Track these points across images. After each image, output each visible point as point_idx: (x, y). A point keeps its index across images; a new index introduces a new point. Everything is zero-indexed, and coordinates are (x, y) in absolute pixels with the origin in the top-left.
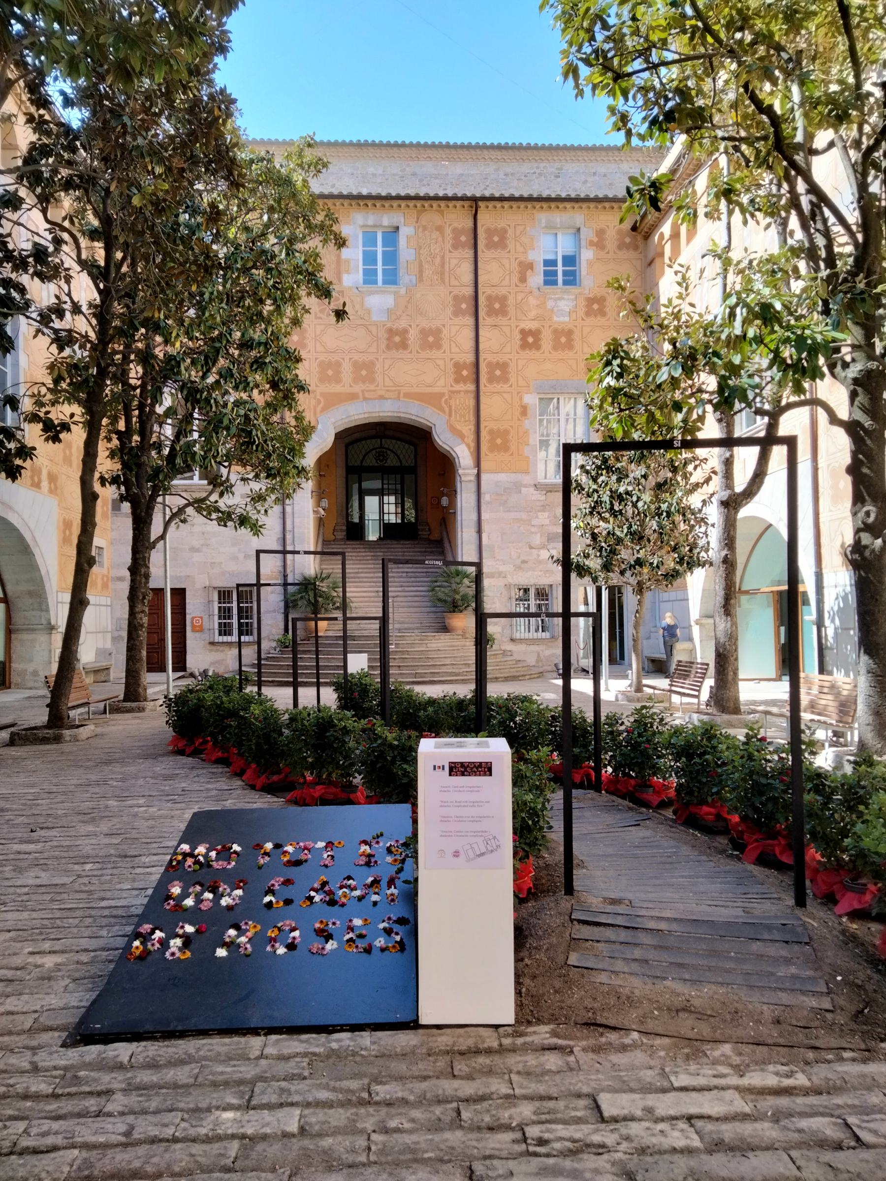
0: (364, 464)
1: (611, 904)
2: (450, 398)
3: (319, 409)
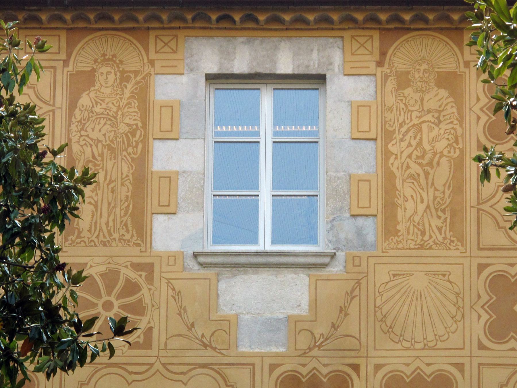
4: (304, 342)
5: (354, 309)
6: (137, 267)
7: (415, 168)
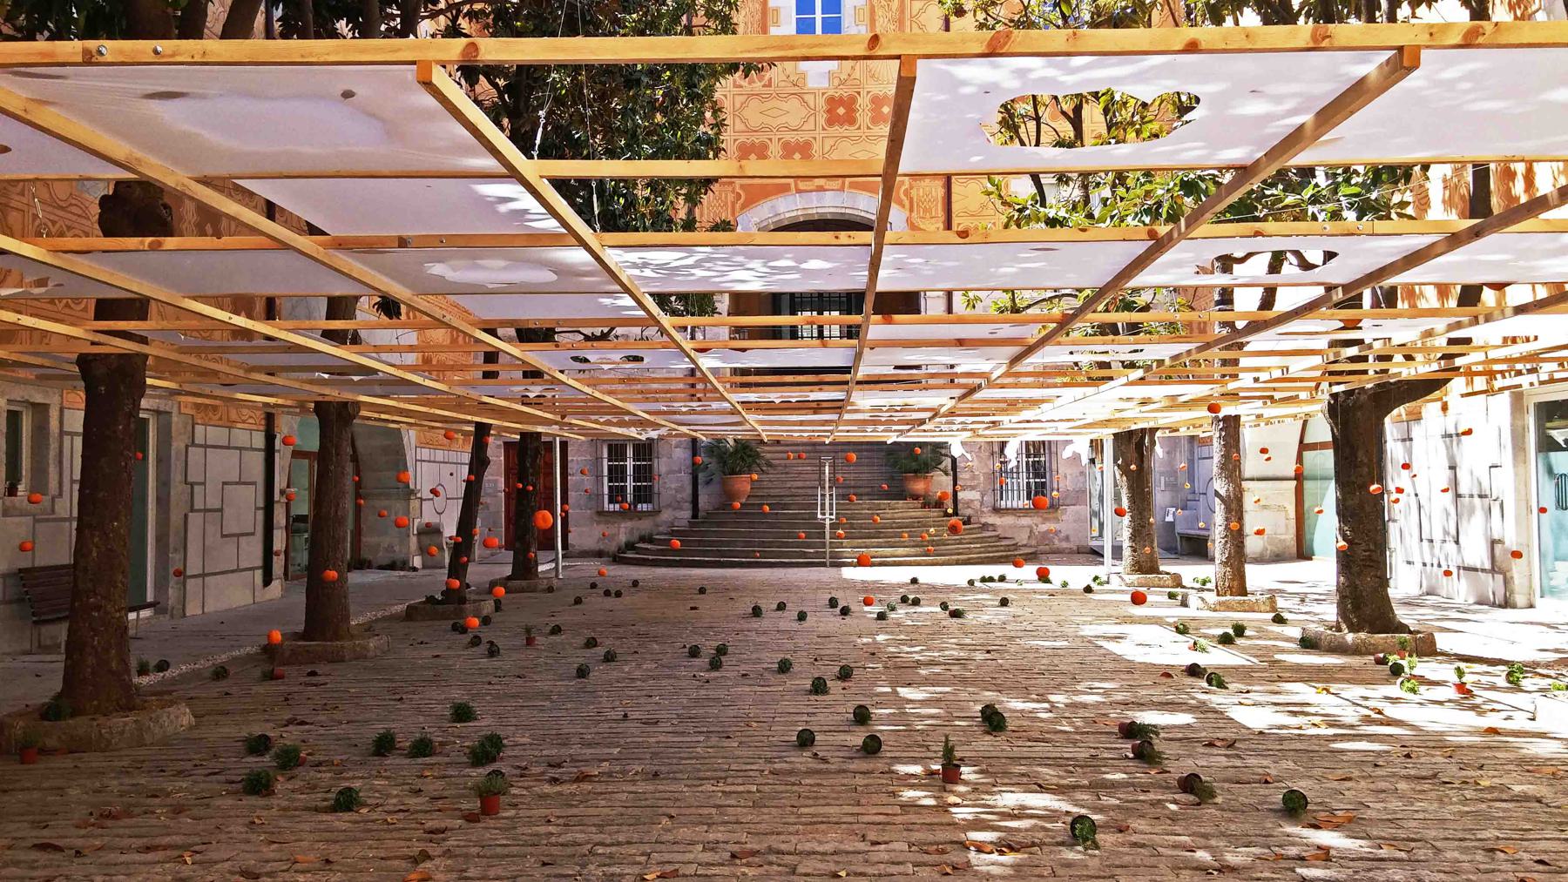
1: (742, 375)
2: (911, 188)
3: (738, 206)
4: (836, 82)
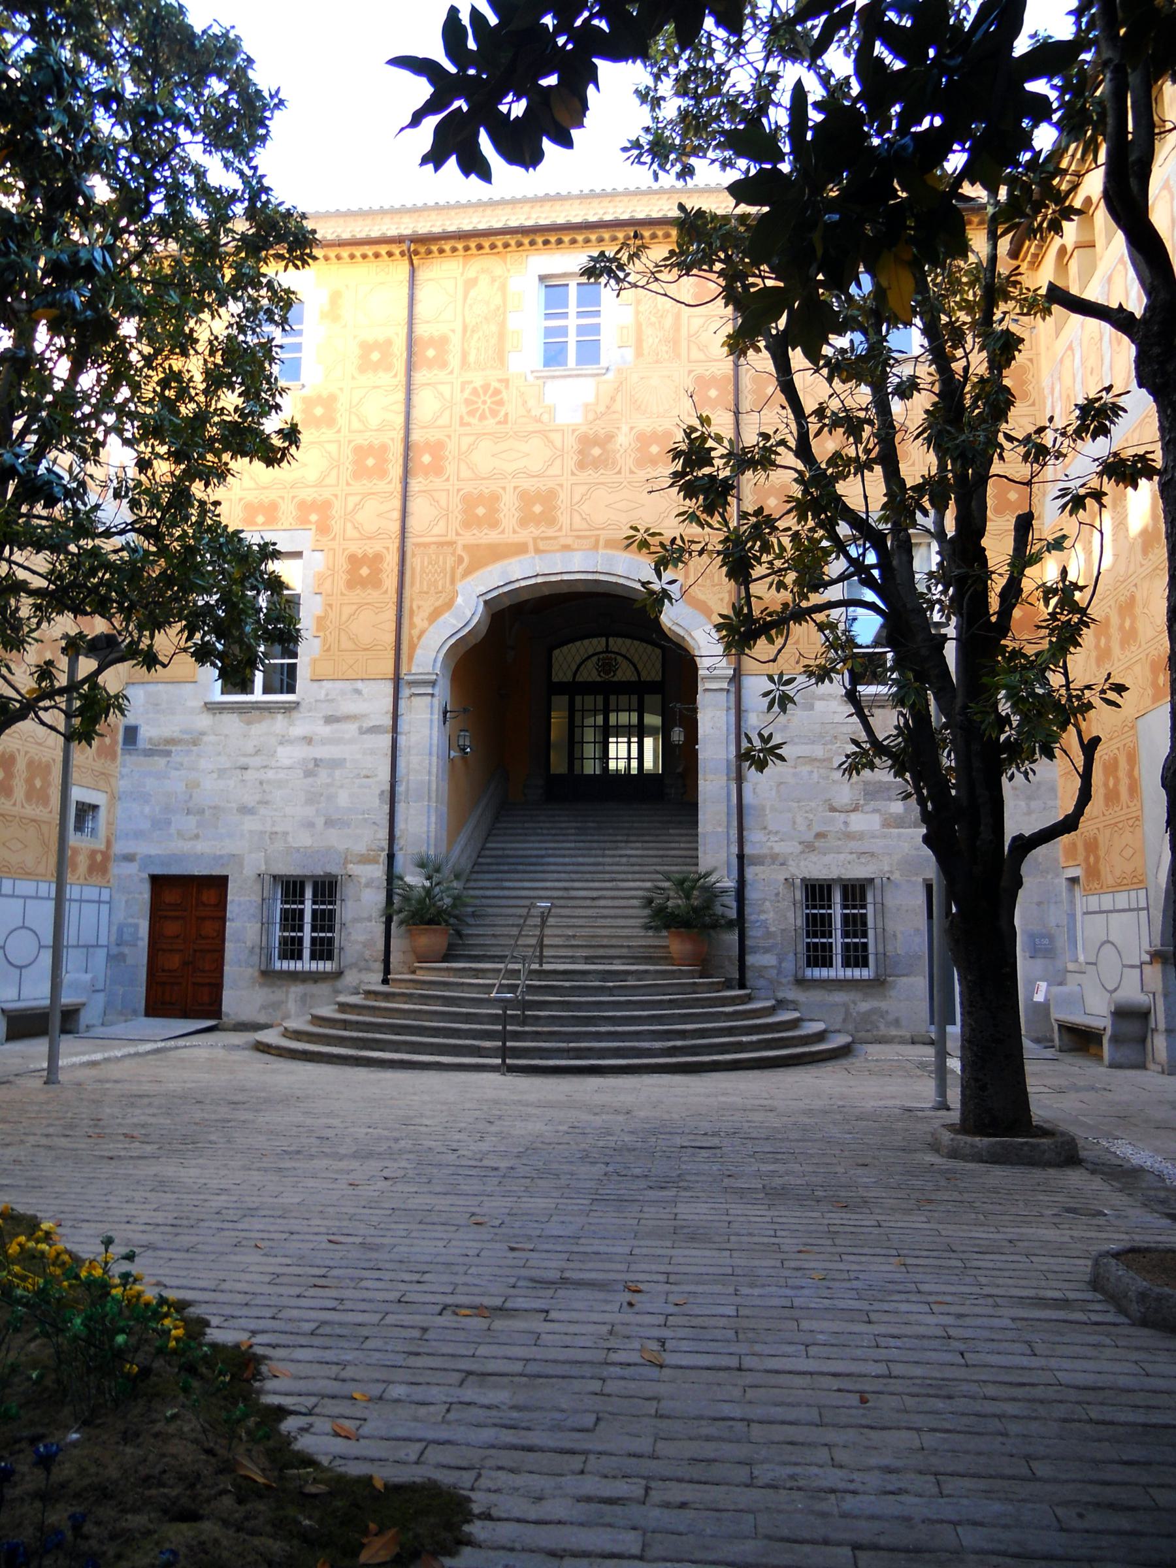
0: (579, 679)
4: (591, 417)
5: (619, 398)
6: (500, 381)
7: (653, 319)
